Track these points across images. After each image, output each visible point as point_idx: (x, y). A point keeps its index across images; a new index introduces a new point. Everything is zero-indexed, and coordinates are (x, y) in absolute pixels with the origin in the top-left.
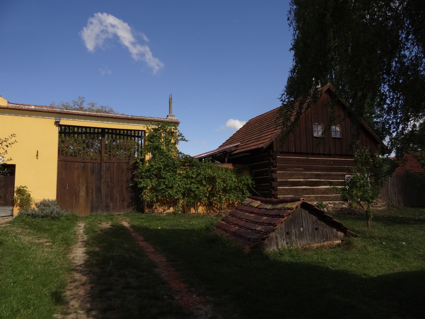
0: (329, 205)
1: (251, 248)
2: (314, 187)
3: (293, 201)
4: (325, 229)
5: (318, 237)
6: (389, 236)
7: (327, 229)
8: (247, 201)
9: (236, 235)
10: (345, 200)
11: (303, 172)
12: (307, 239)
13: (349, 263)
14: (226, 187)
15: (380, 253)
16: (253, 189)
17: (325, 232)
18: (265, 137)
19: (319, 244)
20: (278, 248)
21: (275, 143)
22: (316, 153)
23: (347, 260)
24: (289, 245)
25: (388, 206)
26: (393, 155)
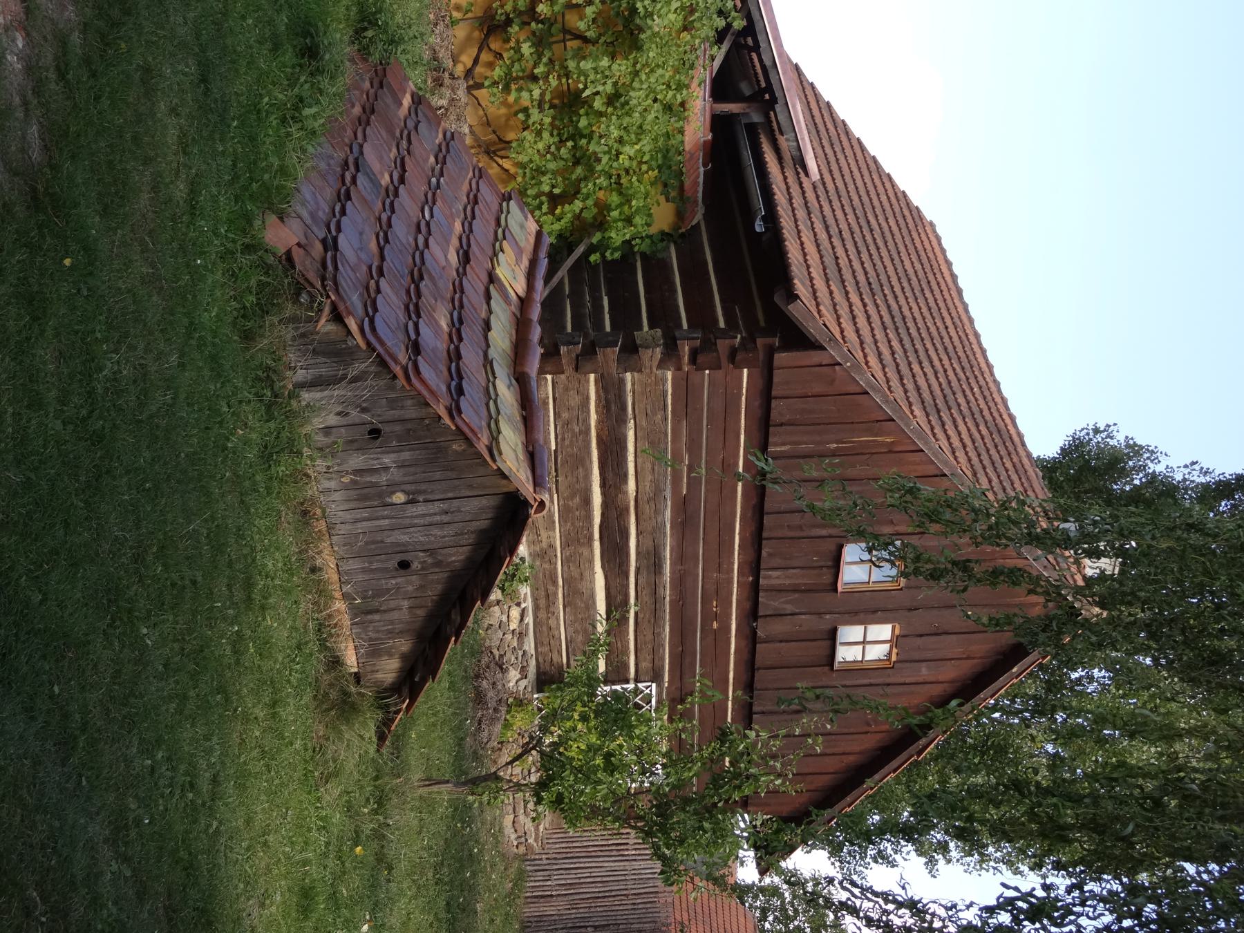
0: (515, 613)
1: (289, 254)
2: (597, 545)
3: (532, 456)
4: (406, 604)
5: (364, 570)
6: (390, 868)
7: (405, 606)
8: (522, 226)
9: (348, 176)
10: (547, 679)
11: (668, 493)
12: (355, 521)
13: (260, 712)
14: (591, 112)
15: (314, 833)
16: (581, 249)
17: (392, 604)
18: (844, 311)
19: (335, 577)
20: (301, 385)
21: (815, 357)
22: (764, 553)
23: (274, 704)
24: (321, 439)
25: (523, 858)
26: (747, 873)
